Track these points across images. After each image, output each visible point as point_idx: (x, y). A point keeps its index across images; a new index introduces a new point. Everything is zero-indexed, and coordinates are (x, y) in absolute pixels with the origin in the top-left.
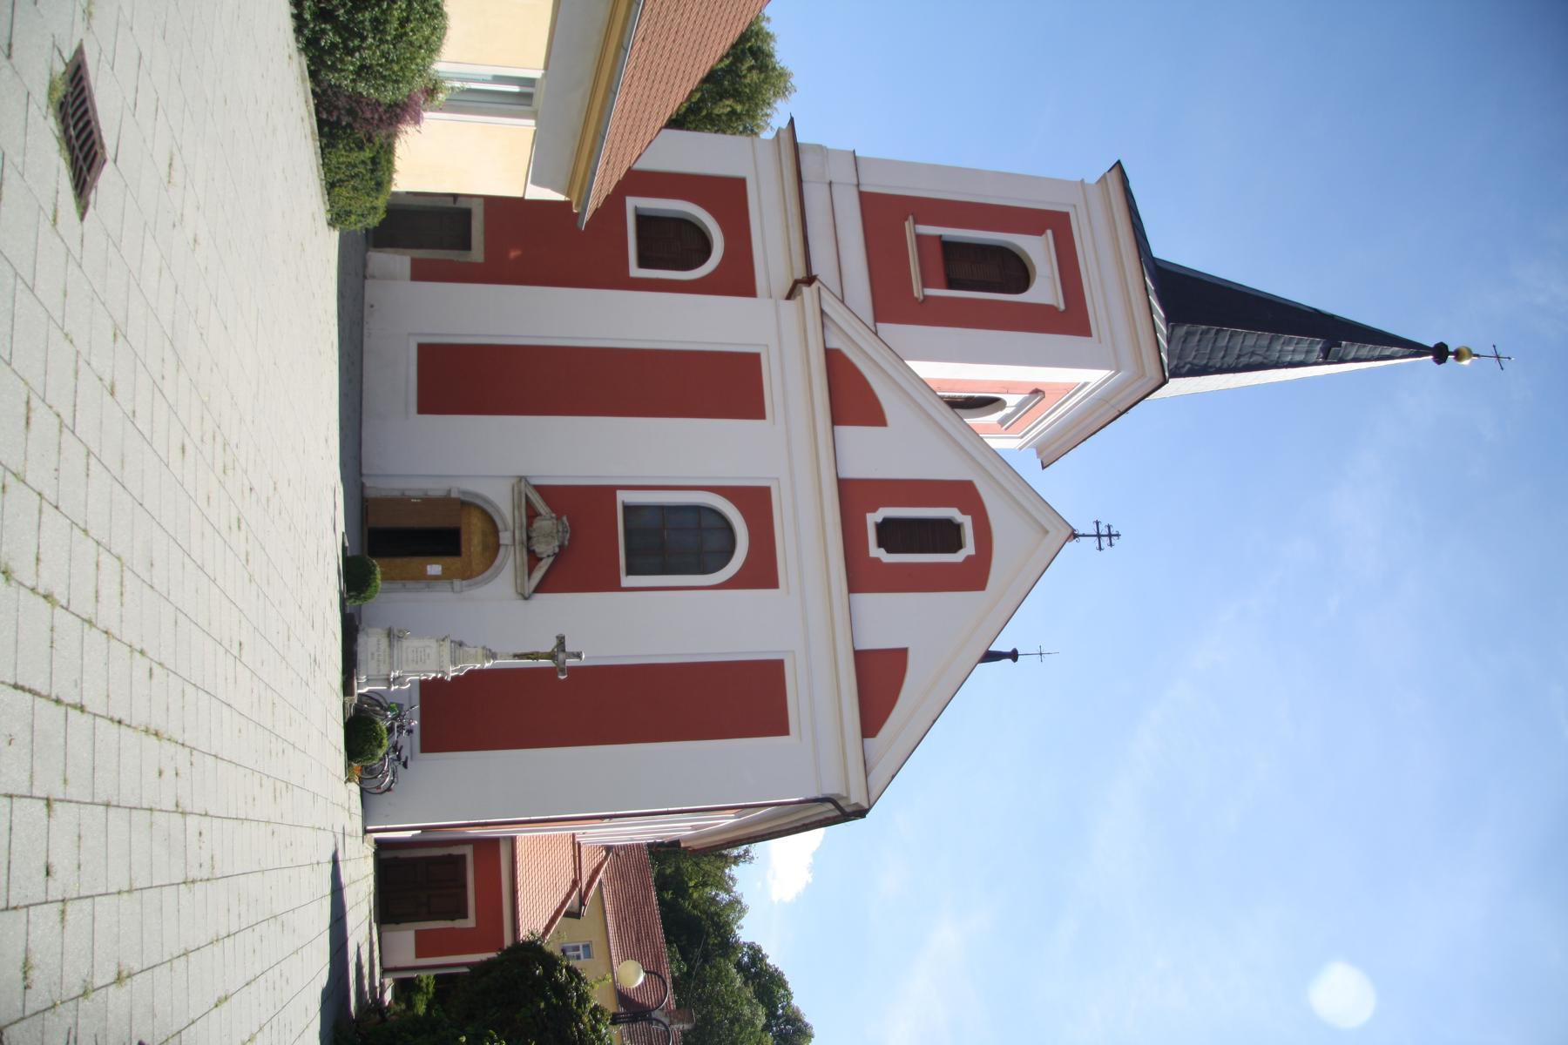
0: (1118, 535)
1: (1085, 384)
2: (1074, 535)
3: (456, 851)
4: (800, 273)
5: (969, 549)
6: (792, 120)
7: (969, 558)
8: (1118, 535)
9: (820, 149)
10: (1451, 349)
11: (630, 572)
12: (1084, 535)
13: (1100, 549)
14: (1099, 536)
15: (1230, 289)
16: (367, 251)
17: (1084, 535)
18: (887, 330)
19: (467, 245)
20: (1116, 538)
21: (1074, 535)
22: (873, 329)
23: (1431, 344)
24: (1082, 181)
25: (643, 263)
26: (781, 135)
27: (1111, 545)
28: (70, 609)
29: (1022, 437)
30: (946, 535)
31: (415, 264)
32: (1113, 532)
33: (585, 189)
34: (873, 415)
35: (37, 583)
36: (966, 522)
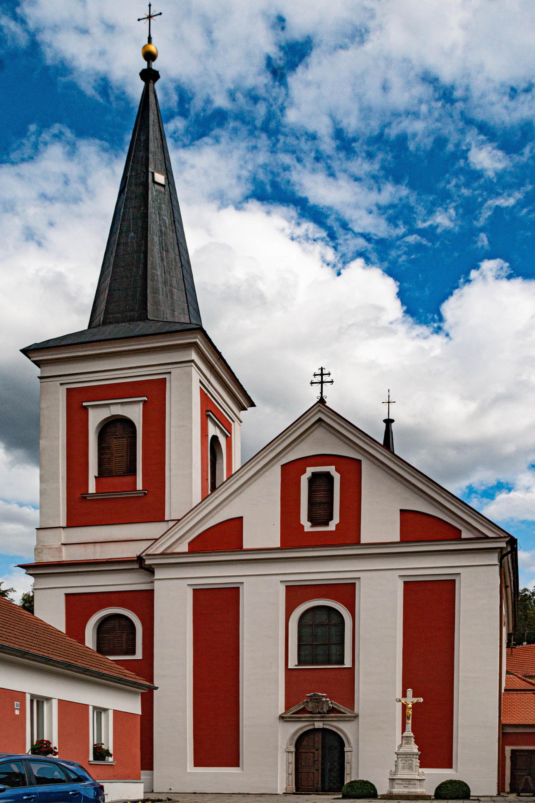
0: (322, 369)
1: (201, 382)
2: (322, 401)
3: (508, 754)
6: (19, 566)
7: (337, 470)
8: (322, 369)
10: (144, 65)
11: (342, 663)
12: (321, 393)
13: (332, 382)
14: (322, 382)
17: (321, 393)
20: (324, 371)
21: (322, 401)
22: (171, 524)
26: (29, 572)
27: (329, 374)
29: (234, 421)
32: (319, 372)
33: (503, 576)
36: (310, 471)
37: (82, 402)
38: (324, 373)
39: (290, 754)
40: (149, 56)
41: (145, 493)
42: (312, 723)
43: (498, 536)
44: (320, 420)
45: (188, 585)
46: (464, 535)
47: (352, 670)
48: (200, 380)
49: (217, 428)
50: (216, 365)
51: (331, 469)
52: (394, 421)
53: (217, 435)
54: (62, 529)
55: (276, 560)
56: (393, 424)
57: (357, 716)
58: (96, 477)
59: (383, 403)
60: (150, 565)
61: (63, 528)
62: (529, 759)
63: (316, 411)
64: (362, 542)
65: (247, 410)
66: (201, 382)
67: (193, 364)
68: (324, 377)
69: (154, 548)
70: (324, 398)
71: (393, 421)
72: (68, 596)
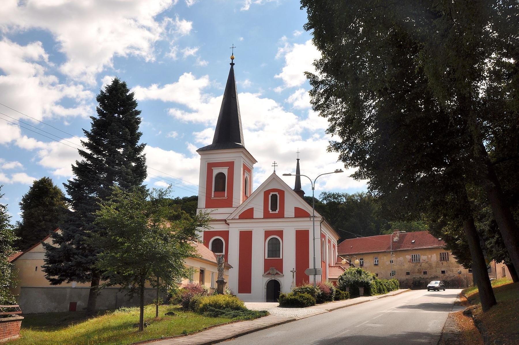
5: (277, 193)
30: (274, 197)
36: (272, 193)
40: (232, 59)
42: (271, 278)
47: (282, 259)
57: (284, 275)
62: (346, 148)
71: (234, 64)
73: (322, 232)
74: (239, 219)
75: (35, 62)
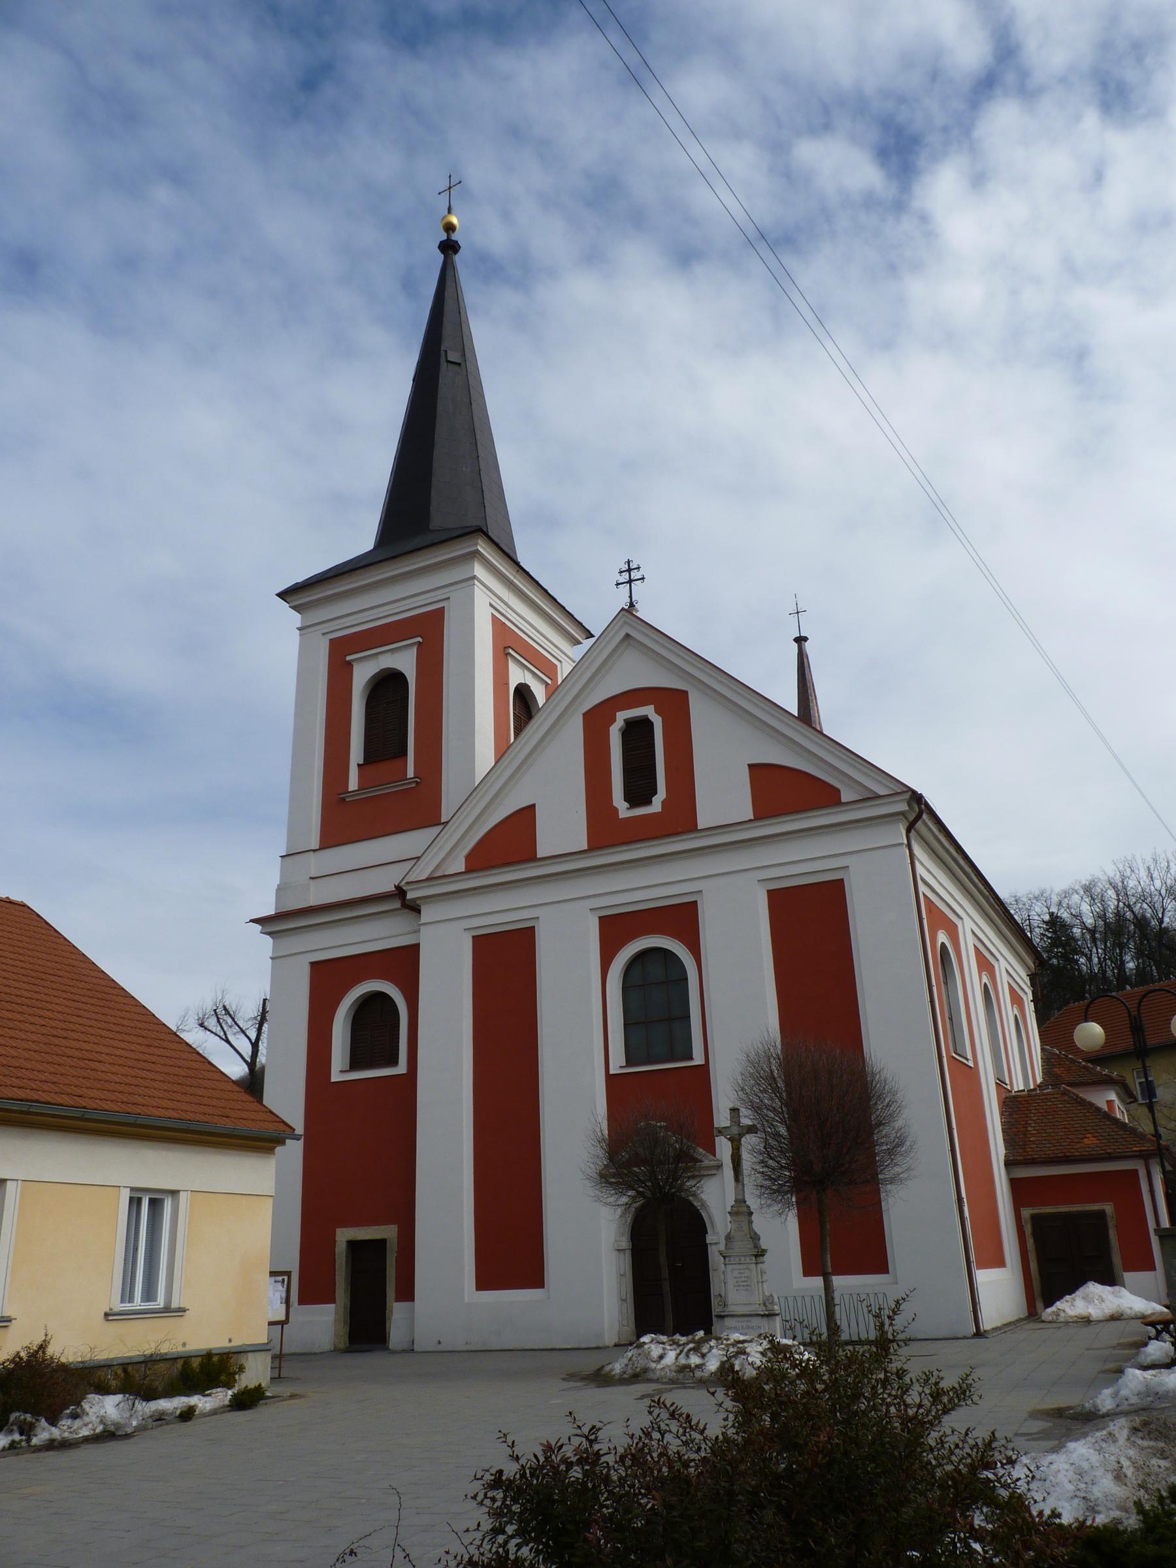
0: (629, 562)
1: (491, 605)
3: (1028, 1229)
4: (397, 904)
6: (253, 921)
7: (657, 711)
9: (280, 890)
10: (444, 237)
11: (691, 1058)
12: (631, 597)
13: (643, 578)
14: (630, 581)
15: (381, 534)
16: (389, 1350)
17: (631, 597)
18: (446, 811)
19: (383, 1242)
20: (631, 565)
21: (630, 608)
23: (441, 257)
24: (299, 629)
25: (393, 1061)
28: (415, 1350)
30: (638, 732)
31: (399, 1299)
34: (527, 814)
35: (394, 1352)
36: (622, 716)
37: (346, 656)
38: (632, 568)
39: (622, 1254)
41: (417, 782)
43: (893, 792)
44: (627, 636)
45: (465, 930)
46: (845, 798)
48: (490, 603)
49: (525, 671)
50: (515, 580)
51: (649, 711)
52: (808, 639)
53: (527, 682)
54: (312, 852)
55: (568, 875)
56: (806, 643)
58: (359, 765)
59: (790, 614)
60: (414, 900)
61: (314, 851)
63: (619, 624)
64: (699, 828)
65: (582, 643)
66: (491, 605)
67: (476, 582)
68: (632, 573)
69: (418, 871)
70: (634, 603)
71: (805, 639)
72: (314, 965)
73: (922, 888)
74: (469, 870)
75: (82, 1442)
